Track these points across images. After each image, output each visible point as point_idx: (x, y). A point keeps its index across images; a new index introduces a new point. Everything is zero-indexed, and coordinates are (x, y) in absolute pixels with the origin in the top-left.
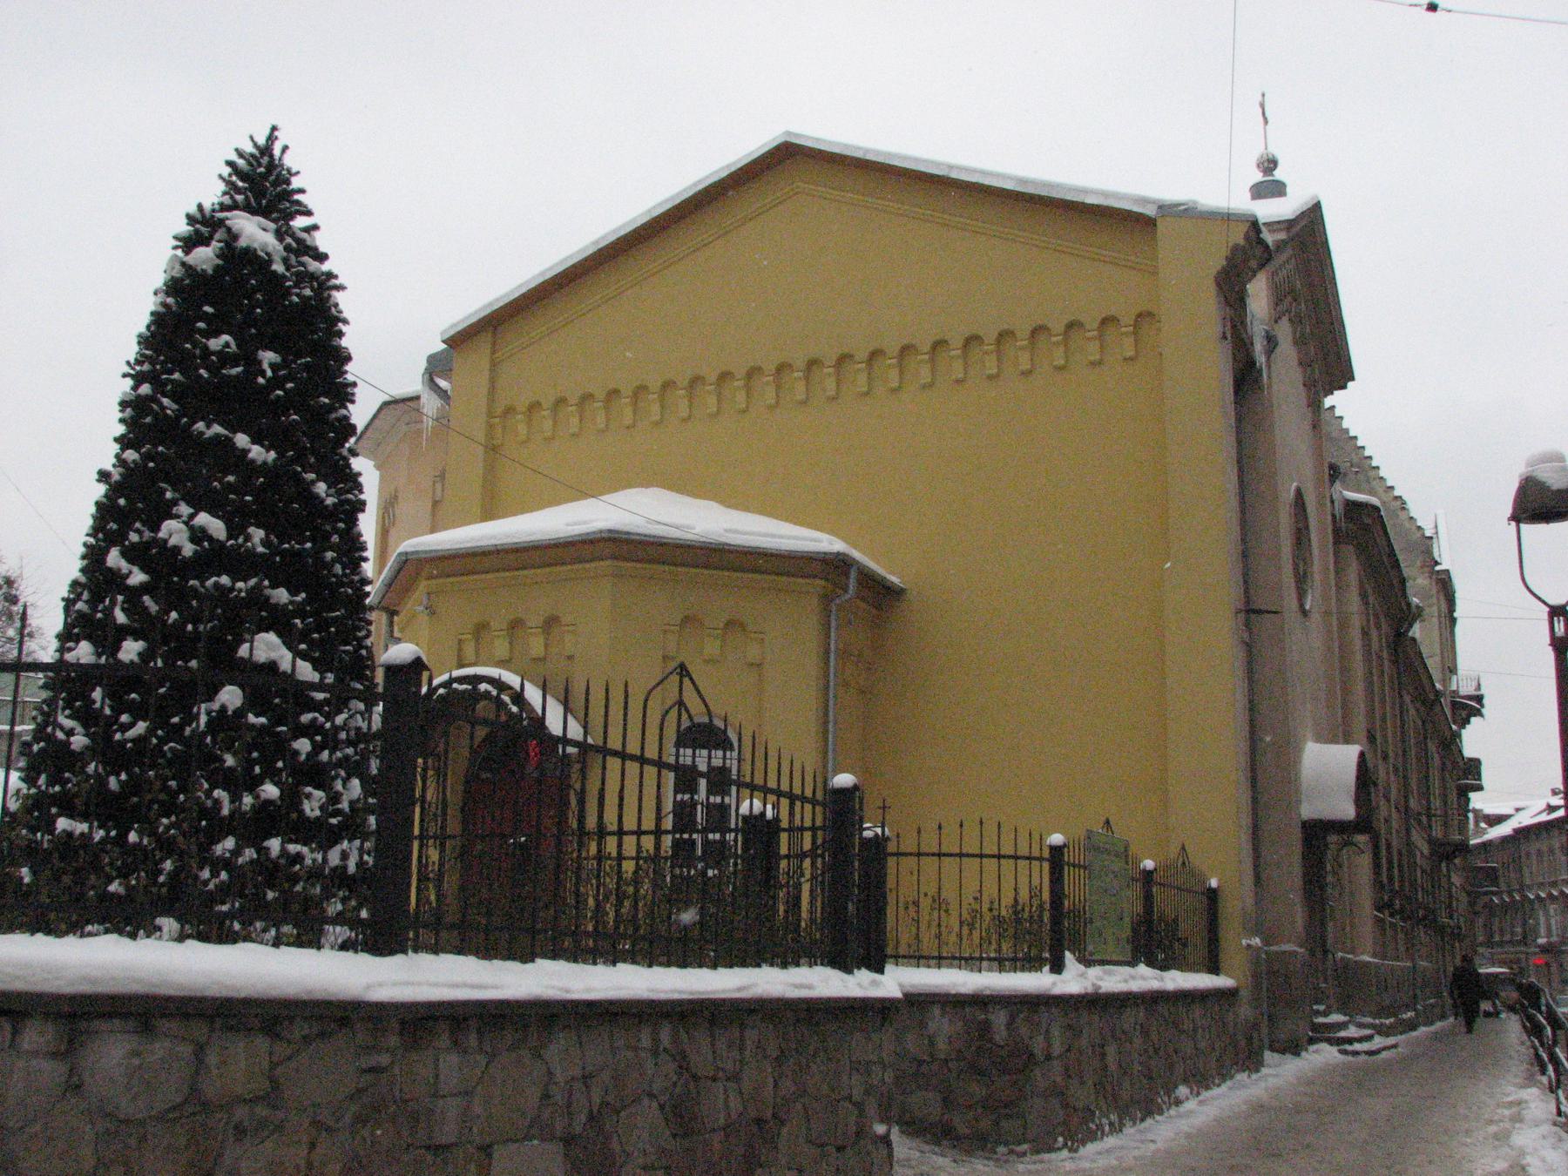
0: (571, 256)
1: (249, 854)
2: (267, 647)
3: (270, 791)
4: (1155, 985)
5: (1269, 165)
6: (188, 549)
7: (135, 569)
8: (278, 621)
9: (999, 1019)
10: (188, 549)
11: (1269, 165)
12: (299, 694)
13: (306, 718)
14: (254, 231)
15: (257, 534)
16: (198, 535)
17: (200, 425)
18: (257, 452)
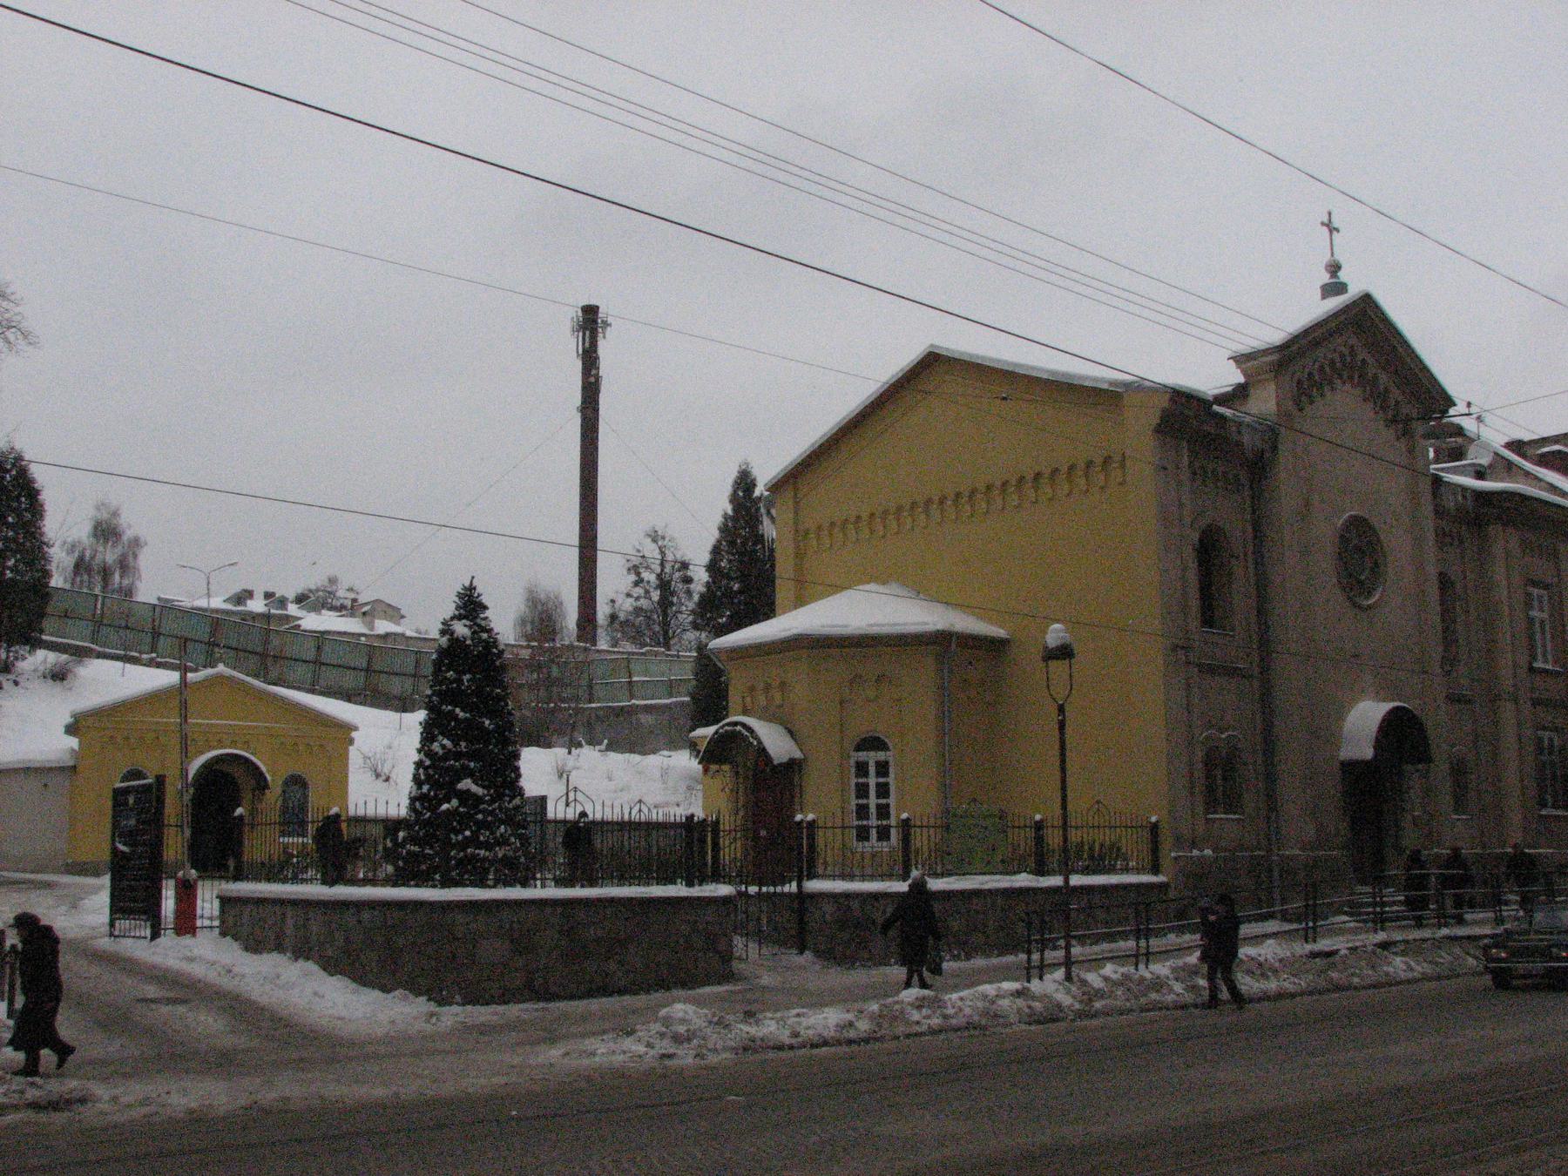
0: (871, 395)
1: (462, 854)
2: (466, 784)
3: (468, 833)
4: (1034, 884)
5: (1334, 268)
6: (441, 752)
7: (427, 760)
8: (470, 774)
9: (855, 904)
10: (441, 752)
11: (1334, 268)
12: (479, 799)
13: (482, 807)
14: (461, 629)
15: (463, 744)
16: (443, 746)
17: (444, 707)
18: (461, 715)
